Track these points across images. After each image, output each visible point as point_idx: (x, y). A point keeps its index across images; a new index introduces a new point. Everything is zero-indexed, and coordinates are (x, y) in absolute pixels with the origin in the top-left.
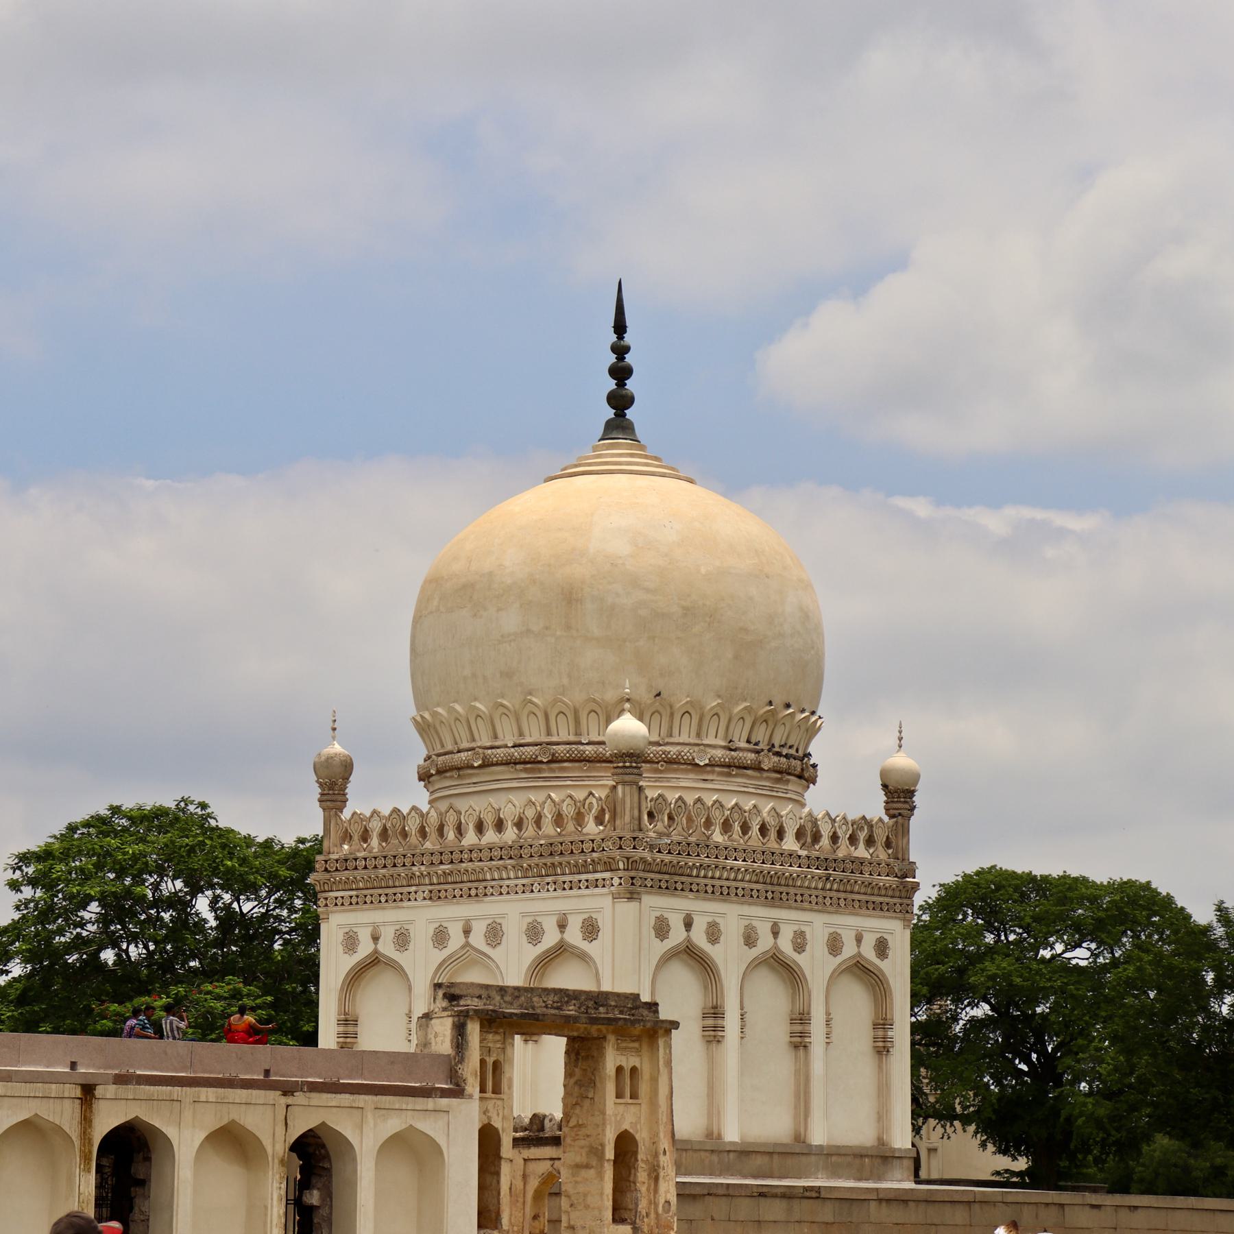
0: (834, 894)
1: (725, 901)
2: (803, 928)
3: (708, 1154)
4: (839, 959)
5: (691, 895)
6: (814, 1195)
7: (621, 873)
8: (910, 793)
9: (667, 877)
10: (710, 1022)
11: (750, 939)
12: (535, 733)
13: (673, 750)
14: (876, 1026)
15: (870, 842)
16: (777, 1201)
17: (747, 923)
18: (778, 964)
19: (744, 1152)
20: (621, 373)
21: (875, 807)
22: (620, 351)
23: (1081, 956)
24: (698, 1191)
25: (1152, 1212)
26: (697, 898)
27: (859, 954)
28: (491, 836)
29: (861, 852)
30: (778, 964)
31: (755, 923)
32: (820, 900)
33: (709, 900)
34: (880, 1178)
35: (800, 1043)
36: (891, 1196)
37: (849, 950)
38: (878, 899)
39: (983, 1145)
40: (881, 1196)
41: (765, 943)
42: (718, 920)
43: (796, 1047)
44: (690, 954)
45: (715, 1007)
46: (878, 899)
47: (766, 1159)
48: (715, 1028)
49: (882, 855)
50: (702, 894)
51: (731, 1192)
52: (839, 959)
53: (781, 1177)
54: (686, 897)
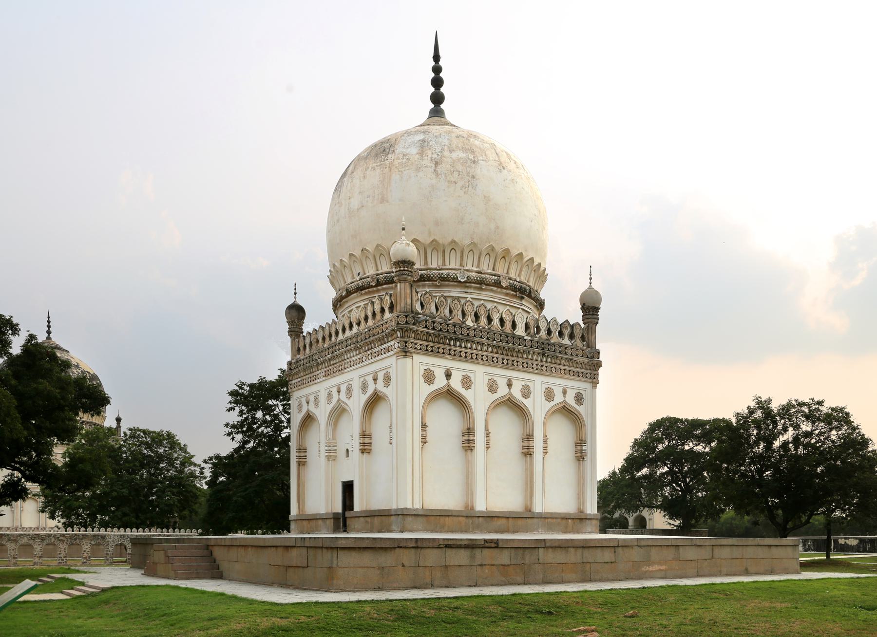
0: (549, 365)
1: (474, 363)
2: (528, 384)
3: (464, 518)
4: (552, 403)
5: (449, 357)
6: (493, 545)
7: (398, 340)
8: (596, 309)
9: (432, 344)
10: (466, 438)
11: (492, 388)
12: (371, 271)
13: (445, 272)
14: (577, 444)
15: (572, 336)
16: (462, 551)
17: (490, 378)
18: (511, 404)
19: (490, 518)
20: (437, 82)
21: (576, 316)
22: (437, 70)
23: (699, 448)
24: (388, 545)
25: (735, 548)
26: (453, 359)
27: (565, 401)
28: (348, 333)
29: (566, 341)
30: (511, 404)
31: (495, 378)
32: (539, 367)
33: (463, 361)
34: (578, 532)
35: (527, 452)
36: (556, 544)
37: (558, 398)
38: (576, 370)
39: (664, 516)
40: (547, 545)
41: (503, 391)
42: (469, 374)
43: (525, 454)
44: (450, 395)
45: (469, 429)
46: (576, 370)
47: (504, 521)
48: (469, 441)
49: (579, 343)
50: (457, 357)
51: (419, 544)
52: (552, 403)
53: (379, 532)
54: (446, 358)
